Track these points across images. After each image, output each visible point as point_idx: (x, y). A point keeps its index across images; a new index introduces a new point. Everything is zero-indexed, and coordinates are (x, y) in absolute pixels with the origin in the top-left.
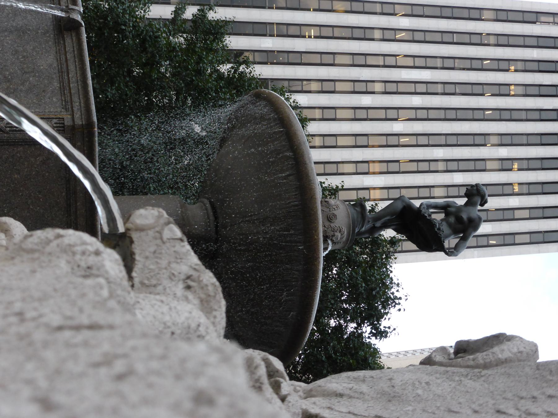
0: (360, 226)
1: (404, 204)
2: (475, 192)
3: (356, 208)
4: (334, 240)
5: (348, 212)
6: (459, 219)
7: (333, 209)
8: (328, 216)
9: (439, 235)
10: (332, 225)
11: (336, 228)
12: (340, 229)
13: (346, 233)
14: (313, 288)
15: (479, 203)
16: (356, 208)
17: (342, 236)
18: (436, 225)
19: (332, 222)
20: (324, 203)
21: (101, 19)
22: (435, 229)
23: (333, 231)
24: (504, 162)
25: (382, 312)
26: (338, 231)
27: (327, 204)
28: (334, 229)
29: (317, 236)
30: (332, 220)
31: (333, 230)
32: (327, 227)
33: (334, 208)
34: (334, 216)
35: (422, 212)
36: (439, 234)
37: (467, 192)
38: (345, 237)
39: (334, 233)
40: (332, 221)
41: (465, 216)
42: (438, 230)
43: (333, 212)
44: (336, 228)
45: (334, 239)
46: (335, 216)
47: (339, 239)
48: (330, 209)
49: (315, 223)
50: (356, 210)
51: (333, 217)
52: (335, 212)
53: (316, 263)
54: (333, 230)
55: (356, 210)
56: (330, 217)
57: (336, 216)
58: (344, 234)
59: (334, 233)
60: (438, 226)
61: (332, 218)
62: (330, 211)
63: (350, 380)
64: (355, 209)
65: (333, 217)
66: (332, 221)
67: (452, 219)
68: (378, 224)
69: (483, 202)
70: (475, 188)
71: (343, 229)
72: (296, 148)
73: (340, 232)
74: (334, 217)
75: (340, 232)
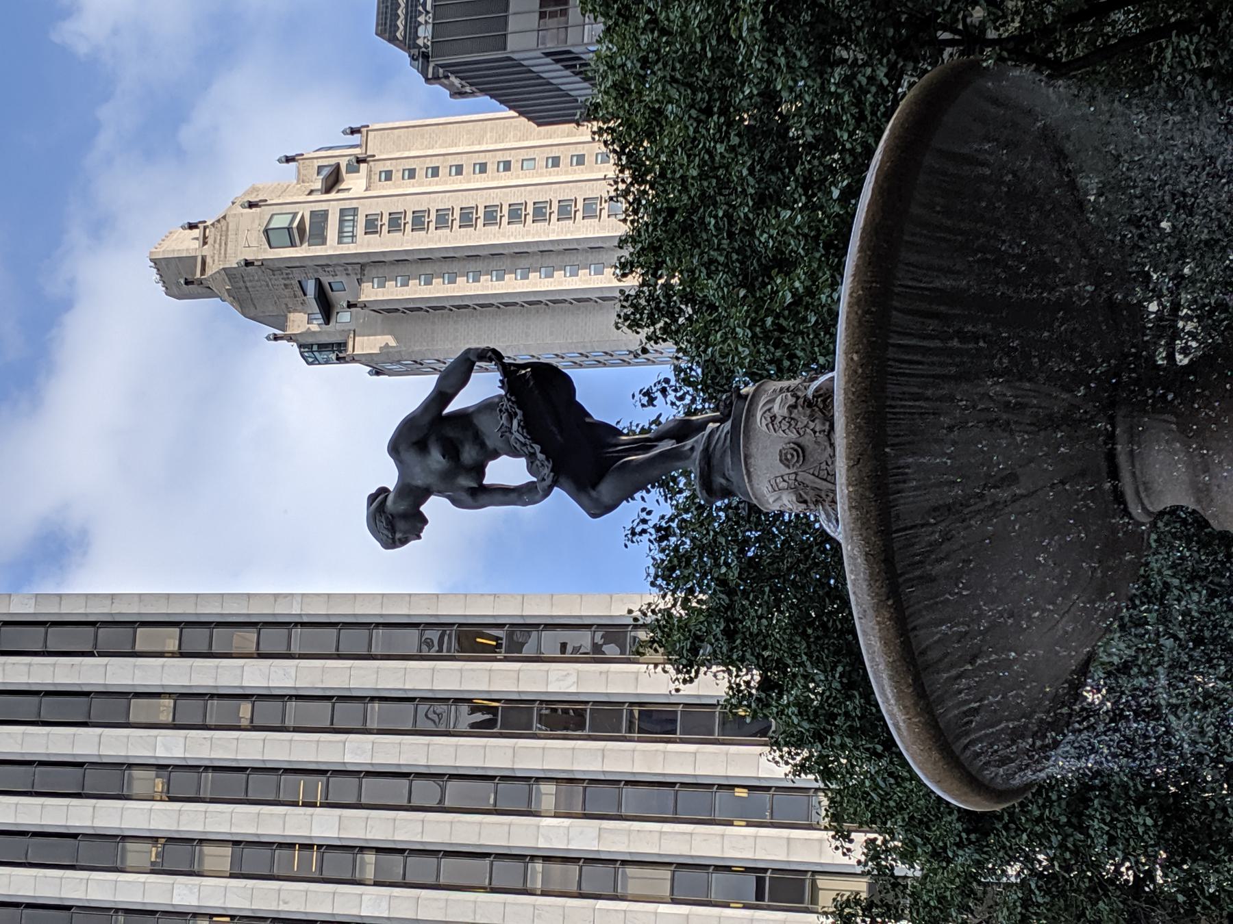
0: (717, 436)
2: (401, 525)
3: (723, 481)
4: (792, 396)
6: (451, 451)
7: (786, 478)
8: (801, 458)
9: (513, 398)
10: (793, 435)
11: (783, 427)
13: (759, 414)
14: (874, 230)
15: (391, 497)
16: (723, 481)
18: (519, 425)
19: (794, 443)
21: (1059, 313)
22: (524, 415)
23: (792, 419)
24: (283, 650)
26: (780, 419)
27: (801, 495)
28: (791, 425)
30: (792, 448)
31: (792, 422)
32: (808, 430)
33: (784, 481)
34: (787, 460)
35: (550, 466)
36: (513, 402)
37: (419, 525)
39: (791, 413)
40: (792, 445)
41: (436, 459)
42: (516, 414)
43: (788, 471)
44: (783, 427)
45: (792, 401)
46: (785, 461)
47: (778, 400)
48: (796, 480)
50: (724, 476)
52: (784, 470)
53: (861, 292)
54: (792, 422)
55: (724, 476)
56: (798, 456)
57: (781, 460)
58: (765, 412)
59: (791, 413)
60: (515, 422)
61: (792, 455)
62: (796, 474)
63: (552, 46)
64: (728, 480)
66: (792, 445)
67: (469, 454)
68: (667, 445)
69: (380, 498)
70: (398, 535)
71: (764, 424)
72: (888, 599)
73: (775, 416)
75: (774, 418)
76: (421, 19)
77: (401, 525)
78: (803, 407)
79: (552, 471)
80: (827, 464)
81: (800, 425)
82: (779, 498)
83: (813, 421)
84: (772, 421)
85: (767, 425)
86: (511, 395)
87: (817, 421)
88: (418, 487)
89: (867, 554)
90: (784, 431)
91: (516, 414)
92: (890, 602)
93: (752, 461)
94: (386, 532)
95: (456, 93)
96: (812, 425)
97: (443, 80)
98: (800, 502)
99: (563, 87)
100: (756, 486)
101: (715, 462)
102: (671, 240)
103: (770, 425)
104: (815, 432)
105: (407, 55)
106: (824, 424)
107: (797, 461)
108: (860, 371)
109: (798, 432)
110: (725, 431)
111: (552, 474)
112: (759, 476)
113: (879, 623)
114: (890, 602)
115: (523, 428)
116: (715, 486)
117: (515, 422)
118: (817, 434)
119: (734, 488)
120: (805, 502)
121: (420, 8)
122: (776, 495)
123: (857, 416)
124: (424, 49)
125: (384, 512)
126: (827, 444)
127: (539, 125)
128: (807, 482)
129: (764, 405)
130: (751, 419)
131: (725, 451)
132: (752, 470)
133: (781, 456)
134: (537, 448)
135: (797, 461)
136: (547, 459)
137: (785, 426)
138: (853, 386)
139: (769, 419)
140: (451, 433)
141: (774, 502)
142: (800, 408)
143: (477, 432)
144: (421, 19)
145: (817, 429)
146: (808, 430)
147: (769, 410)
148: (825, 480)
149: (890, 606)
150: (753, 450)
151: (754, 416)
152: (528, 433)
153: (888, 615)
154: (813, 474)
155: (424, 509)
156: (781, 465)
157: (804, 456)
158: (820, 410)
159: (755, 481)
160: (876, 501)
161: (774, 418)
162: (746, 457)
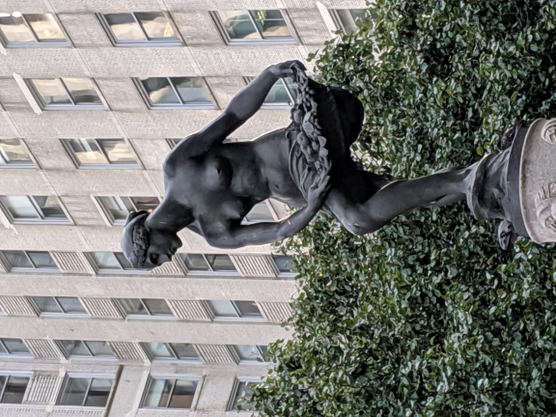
1: (362, 208)
16: (496, 191)
18: (312, 114)
22: (318, 108)
36: (310, 95)
50: (498, 186)
55: (498, 186)
79: (328, 174)
85: (551, 136)
86: (310, 89)
88: (182, 206)
93: (530, 167)
94: (140, 243)
100: (528, 193)
102: (354, 406)
111: (328, 177)
112: (534, 182)
115: (315, 117)
116: (487, 196)
117: (307, 116)
119: (504, 202)
125: (143, 226)
129: (547, 125)
130: (535, 133)
131: (503, 165)
132: (528, 175)
134: (323, 140)
136: (329, 157)
140: (228, 155)
141: (542, 212)
143: (254, 159)
150: (533, 156)
151: (539, 131)
152: (319, 123)
155: (179, 234)
159: (528, 188)
162: (525, 162)
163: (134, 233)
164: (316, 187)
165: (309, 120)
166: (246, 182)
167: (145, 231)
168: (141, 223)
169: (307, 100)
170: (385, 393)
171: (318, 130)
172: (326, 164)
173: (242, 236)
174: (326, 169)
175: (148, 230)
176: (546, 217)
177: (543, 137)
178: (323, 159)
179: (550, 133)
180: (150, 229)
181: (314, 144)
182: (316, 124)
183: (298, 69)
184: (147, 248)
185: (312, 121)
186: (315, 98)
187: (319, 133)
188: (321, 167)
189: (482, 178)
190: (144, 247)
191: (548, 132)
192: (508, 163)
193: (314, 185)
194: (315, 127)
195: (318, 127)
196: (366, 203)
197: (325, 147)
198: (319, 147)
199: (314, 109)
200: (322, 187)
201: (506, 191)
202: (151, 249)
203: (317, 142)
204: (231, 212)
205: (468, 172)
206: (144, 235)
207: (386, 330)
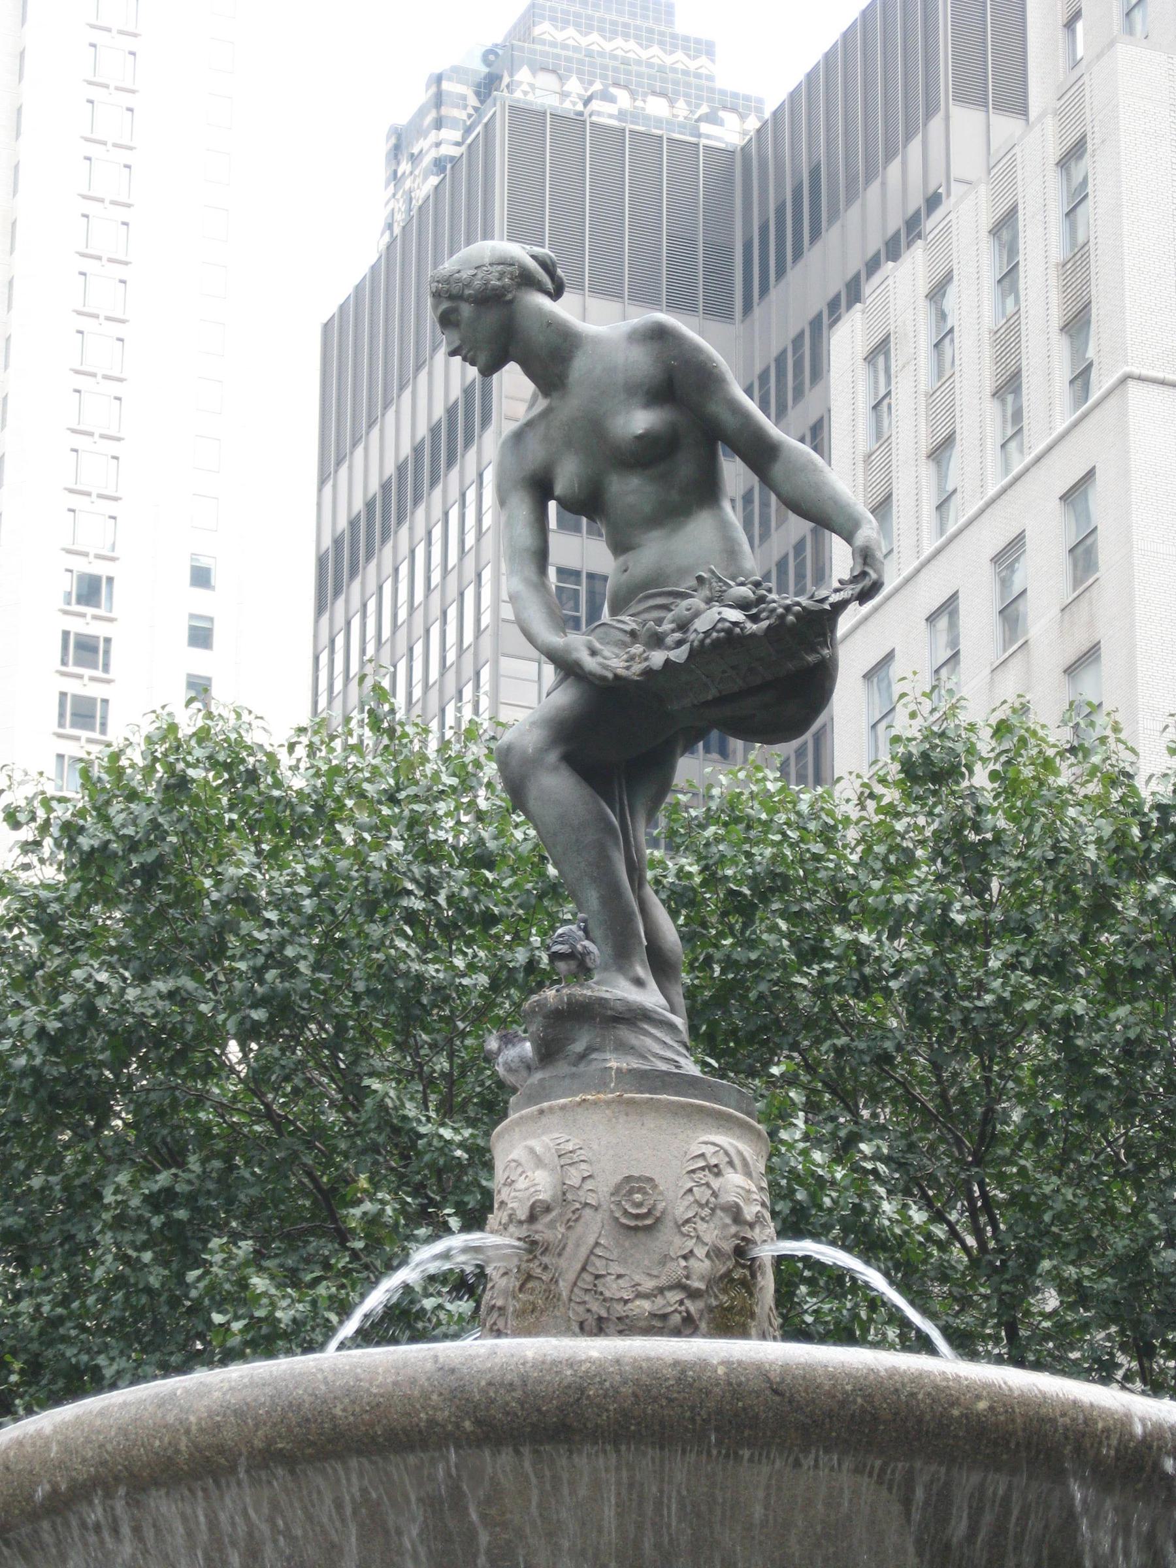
0: (668, 1040)
1: (553, 757)
5: (608, 1103)
7: (589, 1185)
8: (632, 1223)
12: (702, 1169)
13: (723, 1139)
16: (579, 1047)
17: (737, 1161)
18: (736, 624)
20: (539, 1226)
22: (753, 635)
23: (713, 1210)
25: (1113, 1016)
26: (716, 1183)
27: (548, 1209)
29: (978, 1397)
34: (631, 1192)
36: (782, 617)
38: (741, 1146)
46: (631, 1185)
49: (913, 1395)
50: (590, 1049)
51: (638, 1197)
56: (637, 1217)
57: (628, 1179)
58: (727, 1153)
60: (735, 615)
61: (639, 1205)
65: (638, 1197)
71: (709, 1150)
72: (478, 1422)
74: (640, 1190)
76: (574, 85)
77: (491, 318)
78: (735, 1236)
80: (619, 1276)
81: (701, 1226)
82: (539, 1162)
83: (708, 1255)
84: (709, 1168)
85: (702, 1155)
86: (797, 615)
87: (707, 1263)
89: (582, 1390)
90: (690, 1190)
91: (754, 619)
92: (467, 1424)
95: (399, 138)
96: (700, 1252)
97: (433, 114)
98: (533, 1207)
99: (407, 394)
101: (625, 1033)
103: (702, 1164)
104: (685, 1257)
105: (499, 40)
106: (702, 1278)
107: (626, 1213)
108: (956, 1412)
109: (687, 1221)
110: (682, 1061)
111: (610, 675)
113: (426, 1396)
114: (467, 1424)
115: (729, 632)
117: (735, 615)
118: (683, 1263)
120: (532, 1218)
121: (597, 86)
122: (550, 1157)
123: (870, 1398)
124: (506, 80)
125: (519, 286)
126: (663, 1281)
127: (327, 327)
128: (579, 1228)
129: (740, 1153)
131: (645, 1058)
133: (639, 1179)
134: (679, 655)
135: (626, 1212)
137: (702, 1194)
138: (929, 1394)
139: (713, 1161)
141: (532, 1151)
142: (733, 1229)
144: (574, 85)
145: (692, 1262)
146: (691, 1243)
147: (731, 1163)
148: (584, 1269)
149: (458, 1426)
152: (716, 643)
153: (440, 1416)
154: (597, 1244)
156: (619, 1178)
157: (636, 1229)
158: (730, 1272)
160: (693, 1420)
161: (715, 1170)
163: (500, 268)
164: (593, 653)
165: (722, 620)
166: (631, 499)
167: (504, 289)
168: (526, 280)
169: (773, 610)
170: (159, 782)
171: (702, 641)
172: (637, 668)
173: (522, 508)
174: (628, 668)
175: (509, 297)
176: (523, 1161)
177: (705, 1138)
178: (646, 659)
179: (708, 1155)
180: (511, 302)
181: (678, 636)
182: (715, 635)
183: (859, 587)
184: (467, 299)
185: (720, 625)
186: (778, 631)
187: (696, 643)
188: (631, 658)
189: (609, 1013)
190: (467, 292)
191: (713, 1149)
192: (647, 1067)
193: (598, 645)
194: (707, 633)
195: (708, 641)
196: (563, 766)
197: (668, 661)
198: (670, 649)
199: (751, 627)
200: (590, 664)
201: (582, 1068)
202: (466, 310)
203: (679, 643)
204: (567, 477)
205: (639, 983)
206: (494, 289)
207: (376, 1163)
